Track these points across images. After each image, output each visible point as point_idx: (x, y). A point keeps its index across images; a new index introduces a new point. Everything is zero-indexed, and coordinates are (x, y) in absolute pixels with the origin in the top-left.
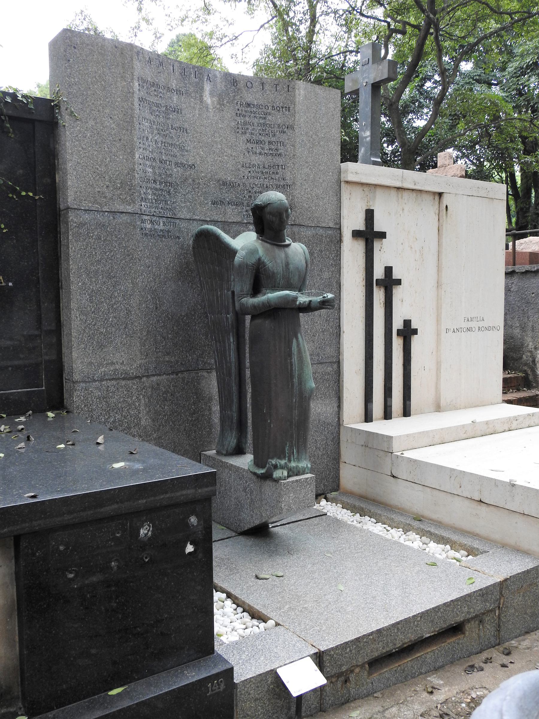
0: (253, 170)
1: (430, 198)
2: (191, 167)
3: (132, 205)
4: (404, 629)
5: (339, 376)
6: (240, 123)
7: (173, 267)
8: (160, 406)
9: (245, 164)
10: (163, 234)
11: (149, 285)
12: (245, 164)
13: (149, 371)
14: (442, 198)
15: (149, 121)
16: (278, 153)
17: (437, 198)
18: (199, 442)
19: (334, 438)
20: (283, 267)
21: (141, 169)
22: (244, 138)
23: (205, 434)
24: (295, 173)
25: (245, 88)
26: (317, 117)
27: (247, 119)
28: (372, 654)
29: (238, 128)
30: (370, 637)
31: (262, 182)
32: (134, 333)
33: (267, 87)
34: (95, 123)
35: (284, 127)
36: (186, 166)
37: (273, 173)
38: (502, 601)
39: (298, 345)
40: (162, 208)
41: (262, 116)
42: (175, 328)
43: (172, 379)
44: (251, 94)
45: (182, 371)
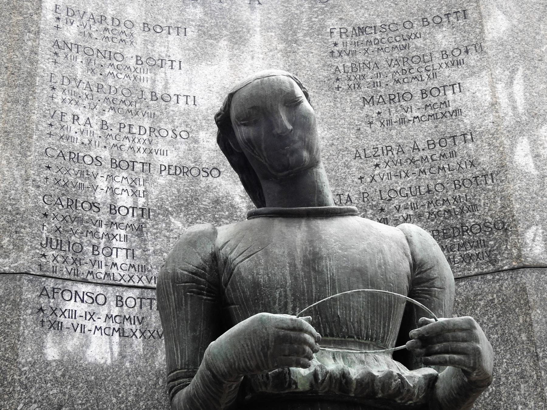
0: (387, 159)
3: (13, 255)
6: (341, 68)
9: (361, 151)
12: (361, 151)
22: (356, 96)
24: (501, 142)
29: (338, 79)
31: (414, 183)
35: (457, 53)
36: (194, 172)
41: (397, 44)
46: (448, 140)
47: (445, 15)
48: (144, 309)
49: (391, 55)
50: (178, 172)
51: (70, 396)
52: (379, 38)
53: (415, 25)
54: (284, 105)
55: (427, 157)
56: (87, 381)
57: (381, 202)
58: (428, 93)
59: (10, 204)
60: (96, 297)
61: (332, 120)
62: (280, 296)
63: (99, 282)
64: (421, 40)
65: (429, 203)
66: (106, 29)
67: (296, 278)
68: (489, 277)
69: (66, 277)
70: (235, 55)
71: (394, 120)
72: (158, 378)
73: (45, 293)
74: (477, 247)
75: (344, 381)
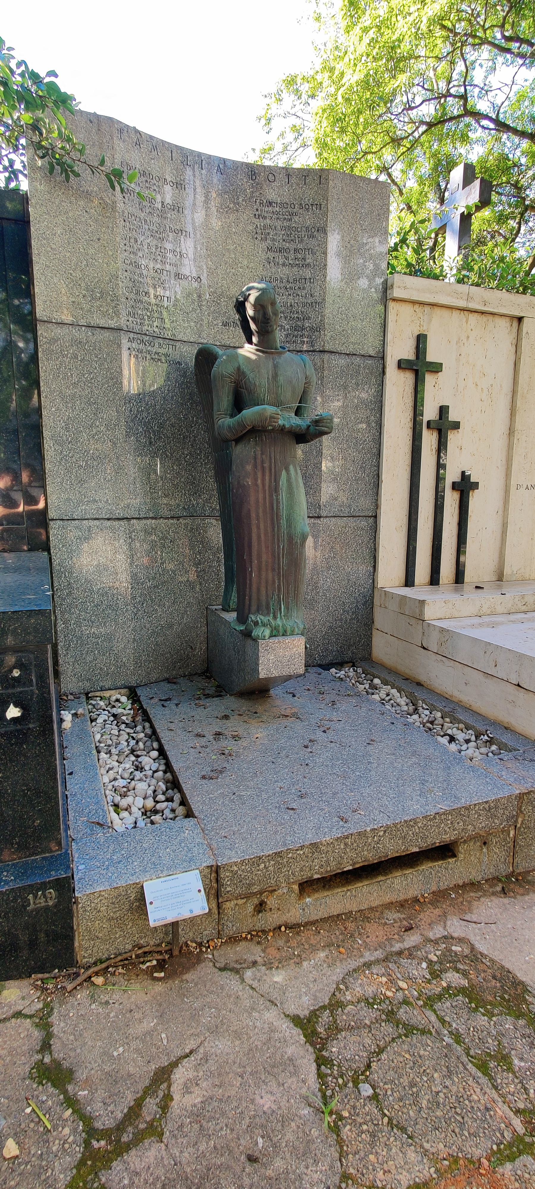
1: (503, 323)
3: (115, 319)
4: (355, 845)
5: (376, 532)
7: (172, 397)
14: (521, 324)
15: (138, 219)
17: (515, 323)
19: (366, 602)
20: (268, 378)
21: (128, 277)
22: (264, 245)
23: (212, 588)
25: (265, 182)
26: (357, 218)
27: (268, 221)
28: (302, 873)
30: (298, 852)
33: (293, 180)
34: (67, 218)
36: (190, 278)
38: (520, 820)
39: (289, 480)
40: (157, 326)
41: (286, 217)
43: (172, 524)
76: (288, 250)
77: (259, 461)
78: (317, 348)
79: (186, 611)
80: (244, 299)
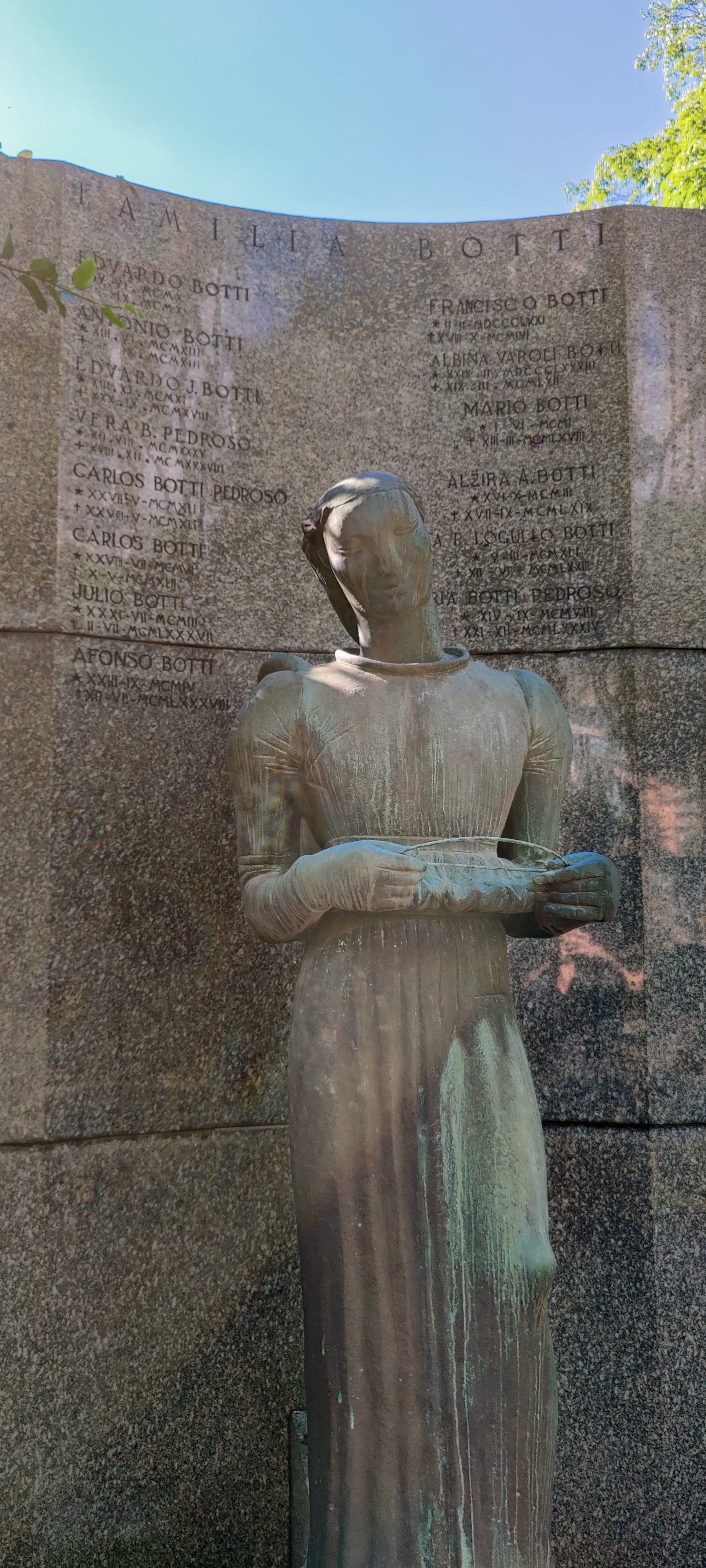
0: (487, 490)
2: (273, 499)
3: (41, 608)
6: (440, 359)
8: (132, 1241)
9: (457, 478)
10: (163, 695)
11: (101, 848)
12: (457, 478)
13: (87, 1122)
16: (571, 430)
18: (288, 1373)
20: (393, 748)
22: (456, 400)
31: (517, 525)
32: (31, 998)
36: (256, 496)
37: (555, 493)
42: (200, 984)
43: (184, 1150)
44: (480, 274)
45: (228, 1125)
46: (564, 473)
47: (579, 293)
48: (196, 673)
49: (505, 345)
50: (236, 496)
51: (113, 779)
52: (491, 318)
53: (538, 304)
54: (395, 533)
55: (535, 493)
56: (131, 761)
57: (476, 547)
58: (545, 404)
59: (34, 541)
60: (140, 660)
61: (426, 432)
62: (378, 789)
63: (143, 639)
64: (544, 327)
65: (533, 554)
66: (146, 289)
67: (396, 767)
68: (593, 655)
69: (105, 634)
70: (309, 332)
71: (500, 438)
72: (211, 756)
73: (79, 656)
74: (584, 615)
75: (446, 901)
76: (519, 406)
77: (363, 1017)
78: (612, 639)
79: (220, 1432)
80: (317, 524)
